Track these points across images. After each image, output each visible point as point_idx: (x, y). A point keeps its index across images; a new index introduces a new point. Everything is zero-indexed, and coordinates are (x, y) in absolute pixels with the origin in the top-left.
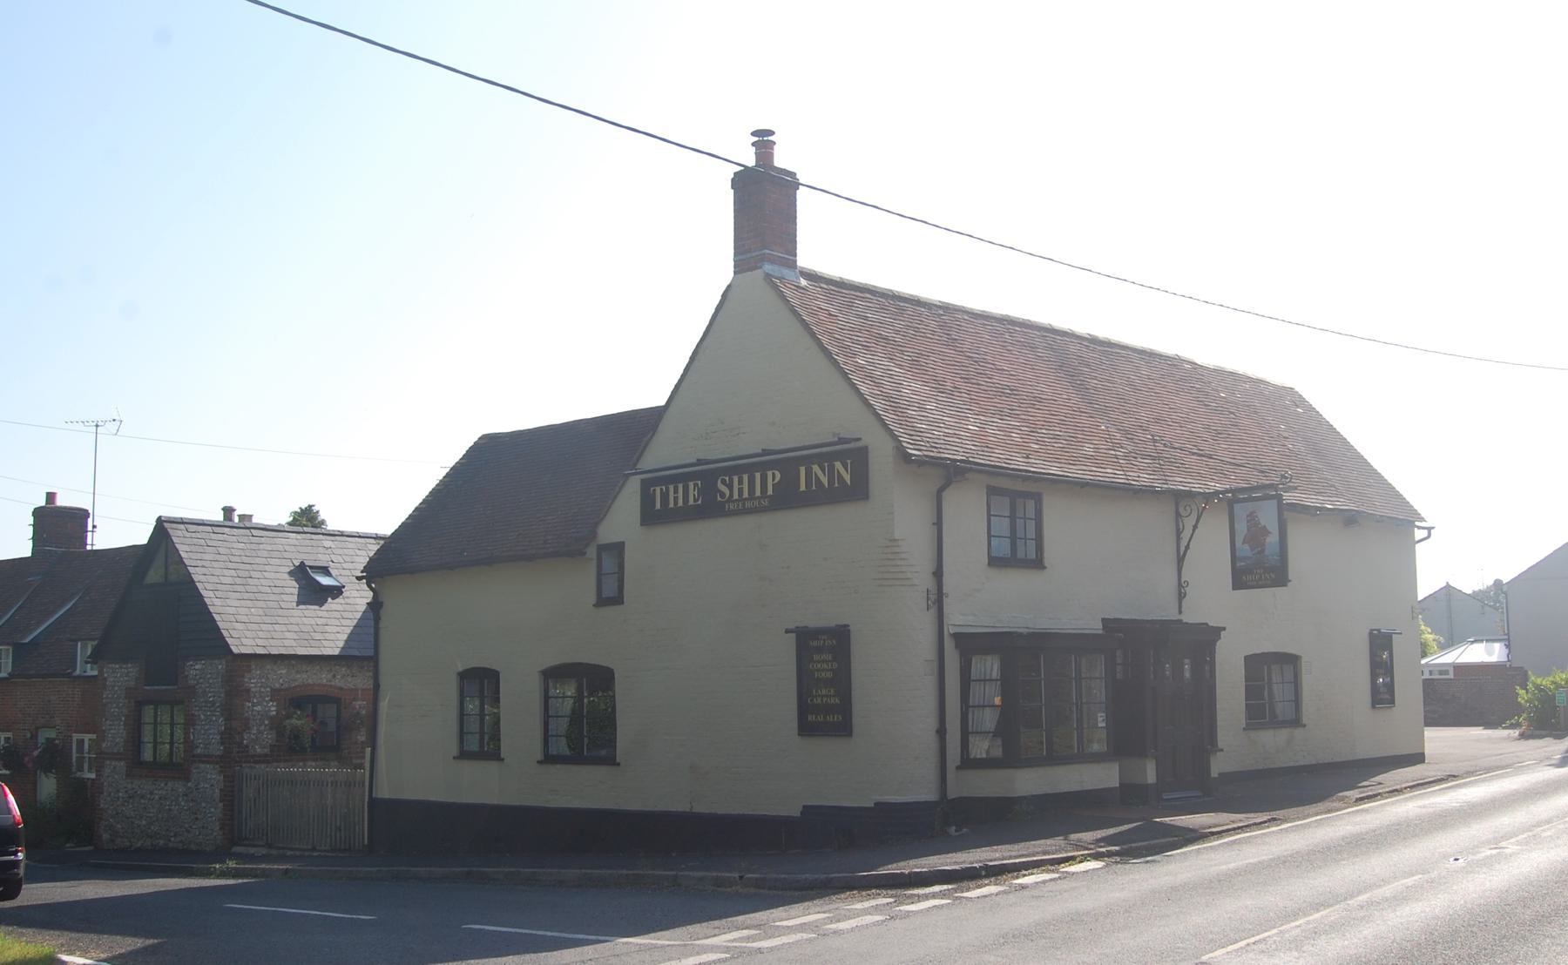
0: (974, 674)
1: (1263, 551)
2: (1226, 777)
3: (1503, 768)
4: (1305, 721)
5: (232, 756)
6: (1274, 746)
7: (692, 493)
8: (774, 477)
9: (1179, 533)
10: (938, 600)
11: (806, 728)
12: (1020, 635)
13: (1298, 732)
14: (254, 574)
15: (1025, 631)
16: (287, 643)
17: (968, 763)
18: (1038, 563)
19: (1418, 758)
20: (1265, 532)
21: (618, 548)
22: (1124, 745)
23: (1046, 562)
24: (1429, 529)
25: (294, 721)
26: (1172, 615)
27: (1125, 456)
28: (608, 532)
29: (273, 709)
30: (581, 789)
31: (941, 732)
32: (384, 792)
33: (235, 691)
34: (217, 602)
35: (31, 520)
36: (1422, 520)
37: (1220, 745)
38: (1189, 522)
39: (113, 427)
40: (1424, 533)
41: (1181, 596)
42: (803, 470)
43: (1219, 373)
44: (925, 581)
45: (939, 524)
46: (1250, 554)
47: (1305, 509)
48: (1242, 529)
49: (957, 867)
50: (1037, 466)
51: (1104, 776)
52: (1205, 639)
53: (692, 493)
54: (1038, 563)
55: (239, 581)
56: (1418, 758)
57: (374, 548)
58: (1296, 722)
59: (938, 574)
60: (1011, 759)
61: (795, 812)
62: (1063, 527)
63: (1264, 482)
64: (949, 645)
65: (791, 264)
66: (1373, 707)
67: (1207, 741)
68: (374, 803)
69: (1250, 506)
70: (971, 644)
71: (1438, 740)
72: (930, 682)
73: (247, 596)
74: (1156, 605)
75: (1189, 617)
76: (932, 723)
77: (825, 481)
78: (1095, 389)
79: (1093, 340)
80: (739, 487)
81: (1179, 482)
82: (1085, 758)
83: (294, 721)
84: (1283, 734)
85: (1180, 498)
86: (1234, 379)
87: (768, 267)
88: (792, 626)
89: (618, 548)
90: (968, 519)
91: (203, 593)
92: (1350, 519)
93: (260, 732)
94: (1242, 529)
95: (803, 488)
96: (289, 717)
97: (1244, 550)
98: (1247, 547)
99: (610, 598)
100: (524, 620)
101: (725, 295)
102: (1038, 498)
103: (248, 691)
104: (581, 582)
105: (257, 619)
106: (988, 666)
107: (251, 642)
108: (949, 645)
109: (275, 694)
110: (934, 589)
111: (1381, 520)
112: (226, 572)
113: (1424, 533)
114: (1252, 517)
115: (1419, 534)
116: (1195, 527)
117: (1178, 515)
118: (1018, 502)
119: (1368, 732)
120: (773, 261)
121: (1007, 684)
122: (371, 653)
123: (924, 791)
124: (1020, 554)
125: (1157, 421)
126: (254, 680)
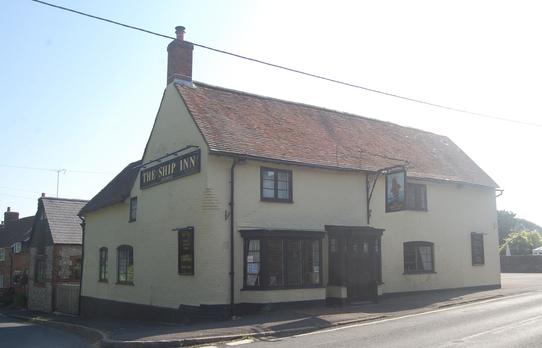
0: (250, 248)
1: (398, 195)
2: (387, 296)
3: (529, 291)
4: (436, 270)
5: (56, 279)
6: (419, 281)
7: (153, 175)
8: (174, 165)
9: (368, 189)
10: (231, 215)
11: (181, 271)
12: (267, 231)
13: (433, 276)
14: (71, 216)
15: (270, 229)
16: (76, 240)
17: (246, 288)
18: (289, 200)
19: (498, 287)
20: (399, 187)
21: (135, 199)
22: (335, 281)
23: (294, 201)
24: (502, 191)
25: (76, 267)
26: (364, 224)
27: (342, 157)
28: (133, 194)
29: (71, 263)
30: (124, 295)
31: (232, 274)
32: (83, 294)
33: (57, 257)
34: (54, 226)
35: (37, 202)
36: (499, 187)
37: (383, 281)
38: (371, 185)
39: (63, 172)
40: (499, 193)
41: (369, 216)
42: (181, 161)
43: (407, 128)
44: (224, 207)
45: (232, 182)
46: (393, 197)
47: (436, 181)
48: (390, 186)
49: (169, 341)
50: (288, 158)
51: (320, 294)
52: (374, 236)
53: (153, 175)
54: (289, 200)
55: (65, 219)
56: (498, 287)
57: (84, 205)
58: (432, 271)
59: (231, 204)
60: (263, 284)
61: (177, 307)
62: (302, 184)
63: (403, 168)
64: (237, 236)
65: (190, 80)
66: (473, 265)
67: (376, 278)
68: (81, 298)
69: (393, 176)
70: (248, 235)
71: (507, 279)
72: (226, 252)
73: (67, 224)
74: (355, 218)
75: (370, 226)
76: (227, 270)
77: (187, 165)
78: (338, 131)
79: (345, 114)
80: (163, 172)
81: (367, 167)
82: (308, 284)
83: (76, 267)
84: (424, 277)
85: (368, 173)
86: (427, 135)
87: (176, 80)
88: (175, 228)
89: (135, 199)
90: (249, 181)
91: (49, 222)
92: (460, 186)
93: (65, 271)
94: (390, 186)
95: (181, 169)
96: (75, 266)
97: (391, 195)
98: (392, 194)
99: (132, 220)
100: (112, 229)
101: (164, 94)
102: (290, 173)
103: (61, 256)
104: (125, 213)
105: (64, 232)
106: (255, 245)
107: (62, 240)
108: (237, 236)
109: (71, 258)
110: (229, 210)
111: (475, 186)
112: (61, 216)
113: (499, 193)
114: (394, 181)
115: (497, 193)
116: (374, 186)
117: (367, 182)
118: (279, 176)
119: (471, 275)
120: (179, 78)
121: (263, 251)
122: (81, 243)
123: (222, 299)
124: (280, 197)
125: (367, 145)
126: (63, 253)
